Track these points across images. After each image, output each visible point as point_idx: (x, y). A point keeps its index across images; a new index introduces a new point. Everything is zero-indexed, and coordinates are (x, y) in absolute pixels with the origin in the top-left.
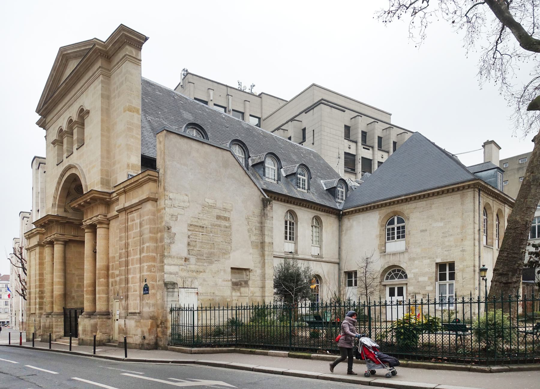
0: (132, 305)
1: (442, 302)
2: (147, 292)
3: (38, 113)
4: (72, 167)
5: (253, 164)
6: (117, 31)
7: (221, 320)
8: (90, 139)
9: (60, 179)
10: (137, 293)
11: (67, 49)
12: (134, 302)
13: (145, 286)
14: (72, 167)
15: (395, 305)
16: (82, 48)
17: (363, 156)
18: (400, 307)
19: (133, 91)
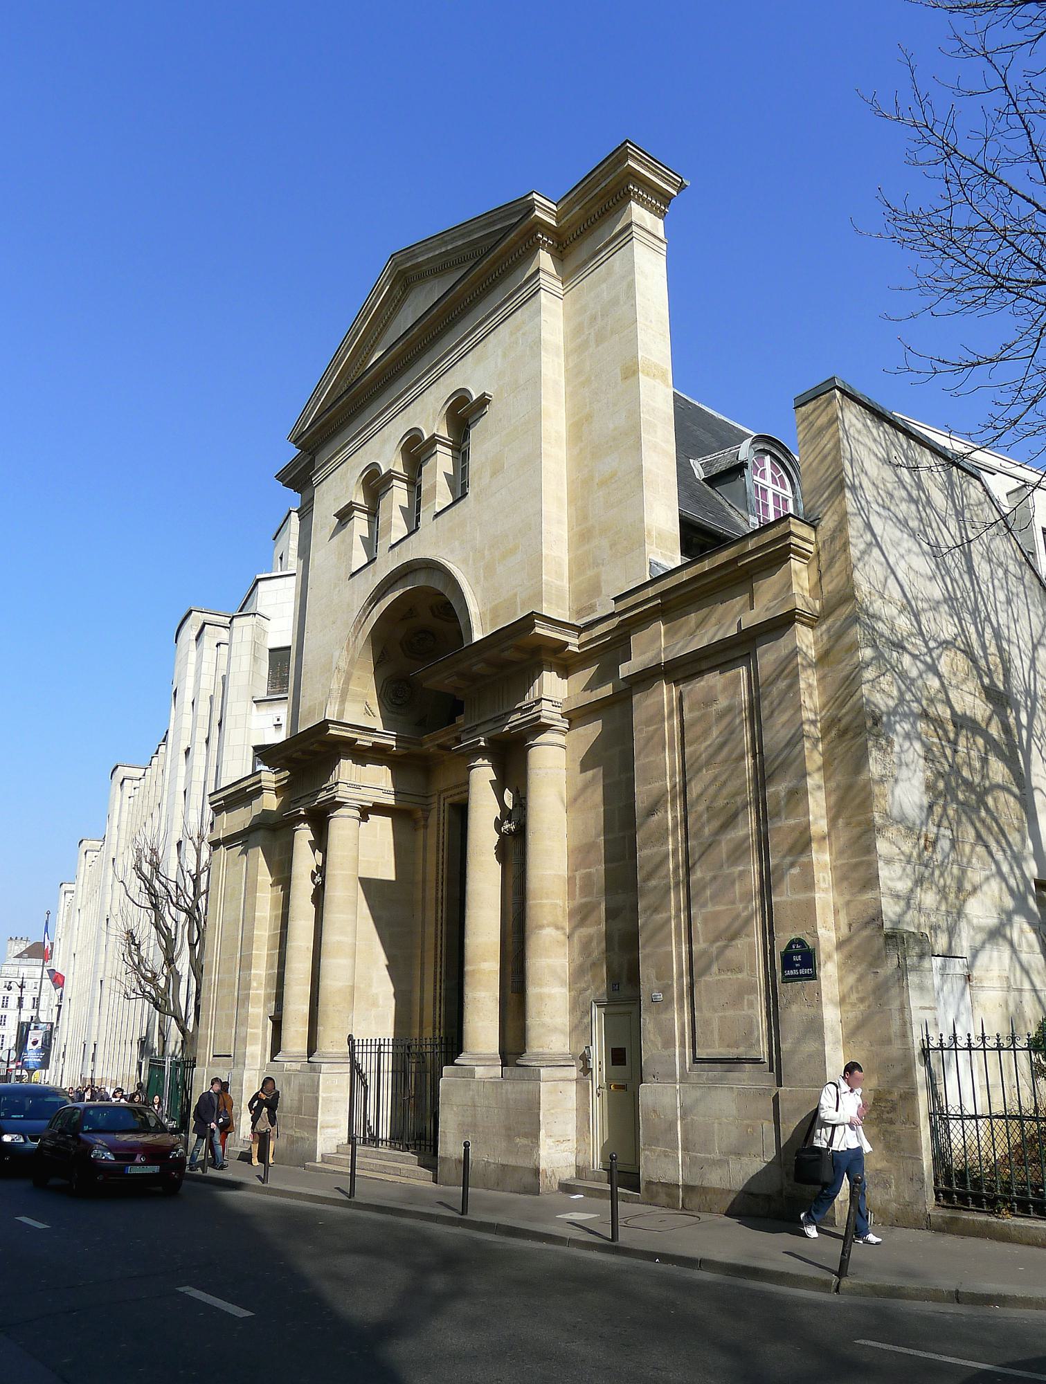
0: (715, 1024)
1: (1014, 1046)
2: (807, 971)
3: (294, 442)
4: (416, 570)
5: (777, 577)
6: (606, 164)
7: (1011, 1094)
8: (494, 474)
9: (364, 612)
10: (740, 976)
11: (417, 251)
12: (730, 1013)
13: (790, 946)
14: (416, 570)
15: (992, 1049)
16: (460, 243)
17: (254, 744)
18: (978, 1056)
19: (651, 321)
